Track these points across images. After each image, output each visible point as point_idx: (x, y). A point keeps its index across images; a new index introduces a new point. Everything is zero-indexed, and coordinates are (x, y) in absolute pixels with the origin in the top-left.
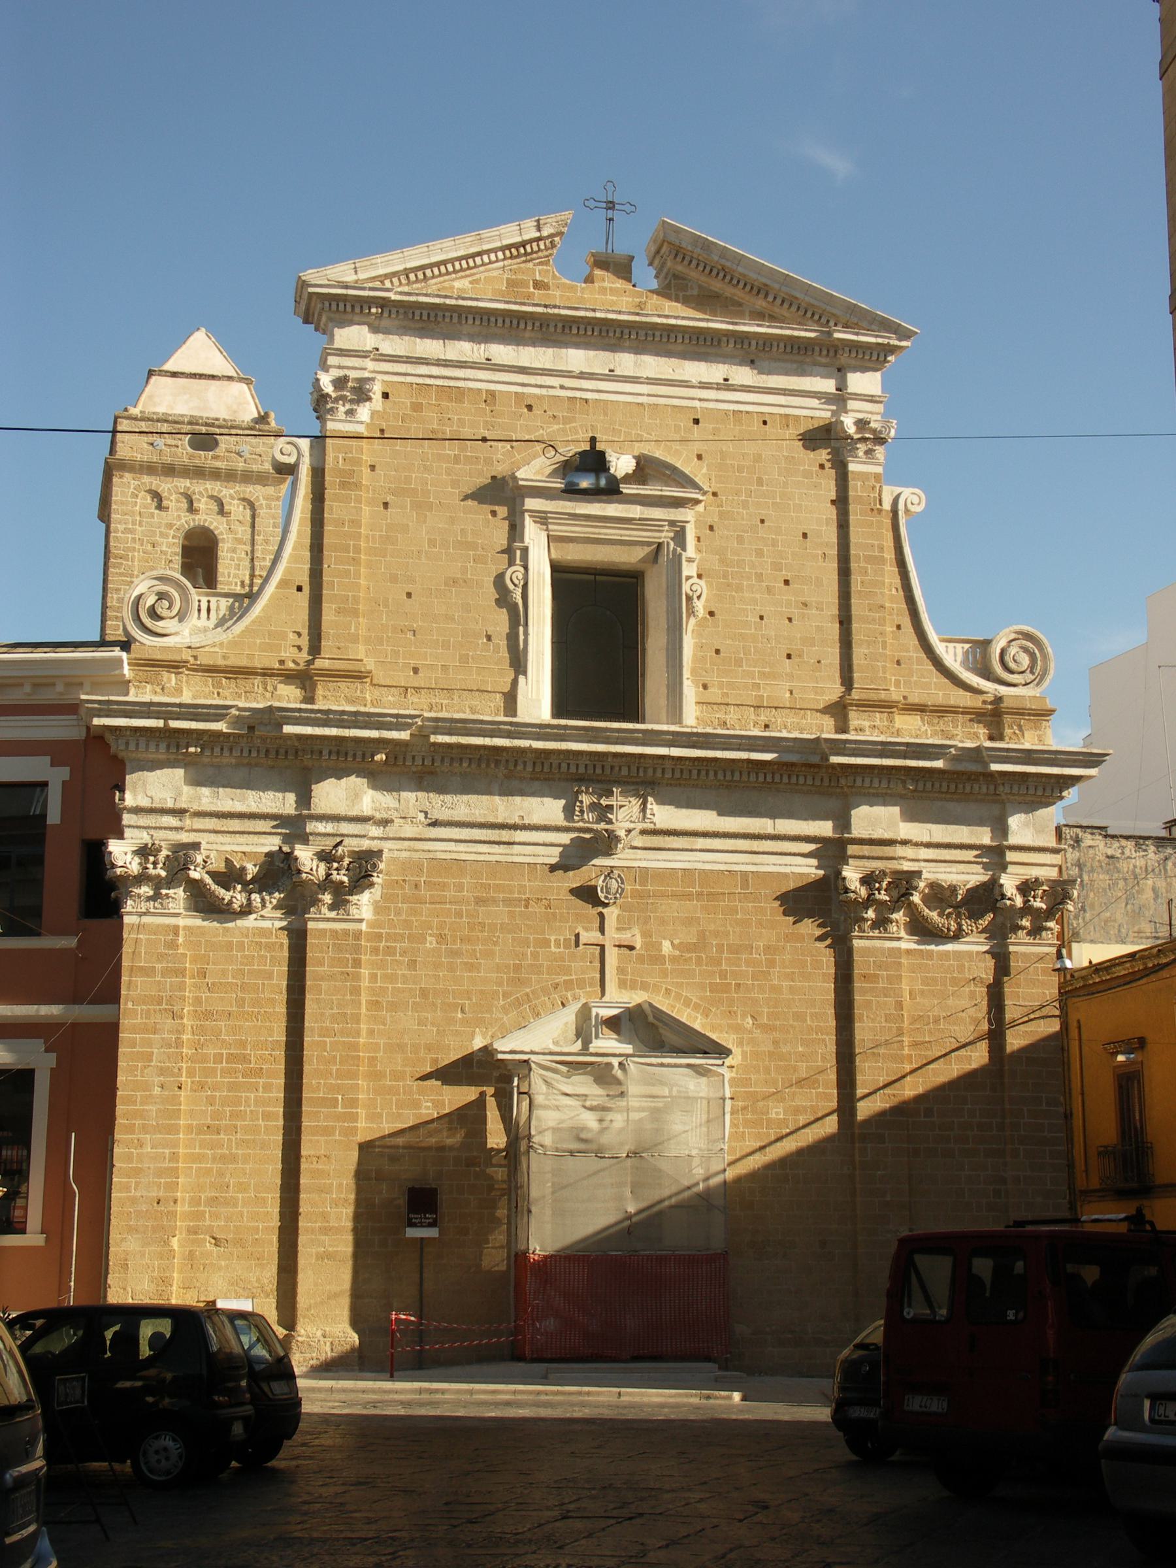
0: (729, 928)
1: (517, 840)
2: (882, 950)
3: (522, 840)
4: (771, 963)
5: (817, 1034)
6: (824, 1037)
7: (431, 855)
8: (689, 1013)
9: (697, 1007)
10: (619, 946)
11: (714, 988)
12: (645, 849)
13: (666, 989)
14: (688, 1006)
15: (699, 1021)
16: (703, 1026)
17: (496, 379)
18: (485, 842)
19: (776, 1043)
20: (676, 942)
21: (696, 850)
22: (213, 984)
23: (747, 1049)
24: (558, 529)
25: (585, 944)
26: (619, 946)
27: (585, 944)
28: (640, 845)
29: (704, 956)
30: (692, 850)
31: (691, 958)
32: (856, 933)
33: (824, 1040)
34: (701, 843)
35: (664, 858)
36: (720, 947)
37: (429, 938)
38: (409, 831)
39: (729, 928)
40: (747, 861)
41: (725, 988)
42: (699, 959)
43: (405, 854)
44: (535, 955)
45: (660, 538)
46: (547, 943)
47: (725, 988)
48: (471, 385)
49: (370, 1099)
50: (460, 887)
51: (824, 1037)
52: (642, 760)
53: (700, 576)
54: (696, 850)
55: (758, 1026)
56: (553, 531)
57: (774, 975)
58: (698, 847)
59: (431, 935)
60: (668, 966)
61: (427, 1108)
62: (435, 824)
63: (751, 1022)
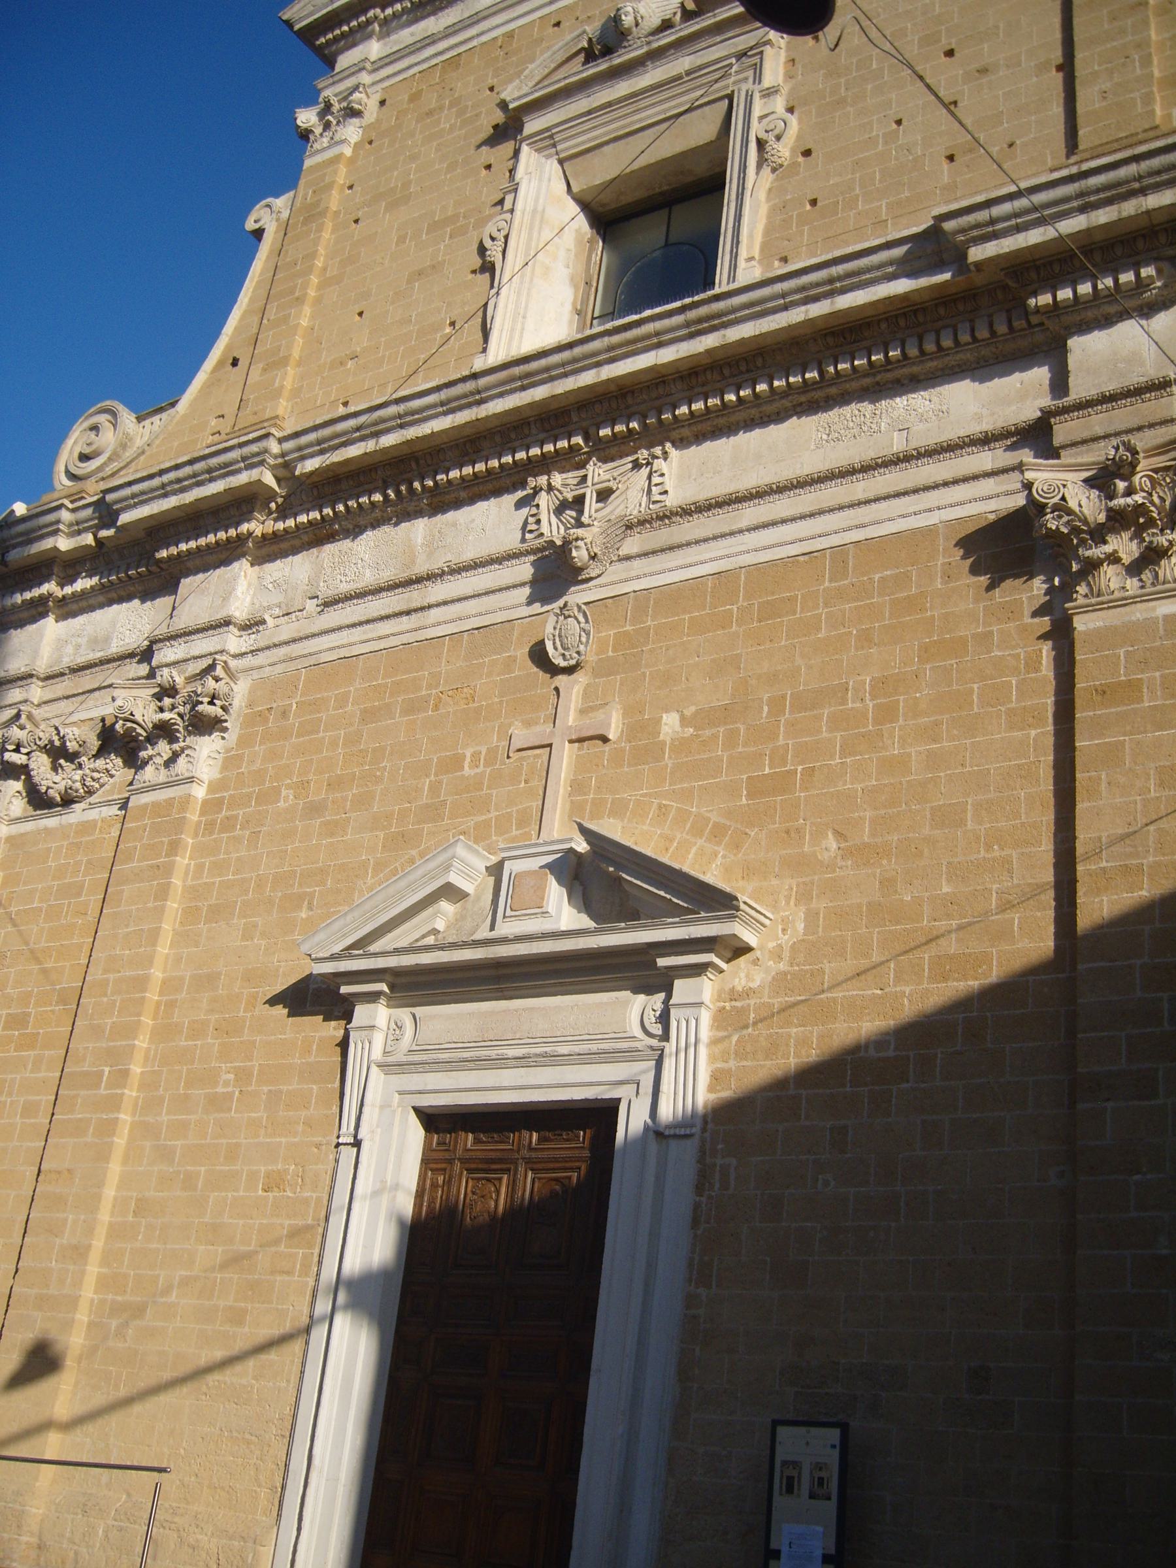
0: (799, 661)
1: (432, 600)
2: (1149, 625)
3: (441, 597)
4: (887, 714)
5: (989, 847)
6: (1007, 852)
7: (312, 660)
8: (701, 849)
9: (718, 833)
10: (581, 740)
11: (757, 788)
12: (645, 554)
13: (660, 807)
14: (697, 831)
15: (719, 860)
16: (727, 870)
17: (515, 15)
18: (382, 618)
19: (887, 884)
20: (689, 711)
21: (741, 531)
22: (18, 913)
23: (821, 904)
24: (567, 147)
25: (519, 750)
26: (581, 740)
27: (519, 750)
28: (635, 550)
29: (742, 728)
30: (732, 534)
31: (715, 737)
32: (1081, 601)
33: (1007, 861)
34: (751, 513)
35: (680, 562)
36: (777, 705)
37: (284, 792)
38: (288, 630)
39: (799, 661)
40: (844, 525)
41: (782, 783)
42: (732, 737)
43: (279, 669)
44: (435, 789)
45: (727, 87)
46: (458, 761)
47: (782, 783)
48: (484, 39)
49: (154, 1072)
50: (342, 701)
51: (1007, 852)
52: (630, 400)
53: (791, 110)
54: (741, 531)
55: (846, 853)
56: (562, 151)
57: (892, 736)
58: (744, 524)
59: (288, 787)
60: (668, 761)
61: (227, 1083)
62: (328, 604)
63: (834, 846)
